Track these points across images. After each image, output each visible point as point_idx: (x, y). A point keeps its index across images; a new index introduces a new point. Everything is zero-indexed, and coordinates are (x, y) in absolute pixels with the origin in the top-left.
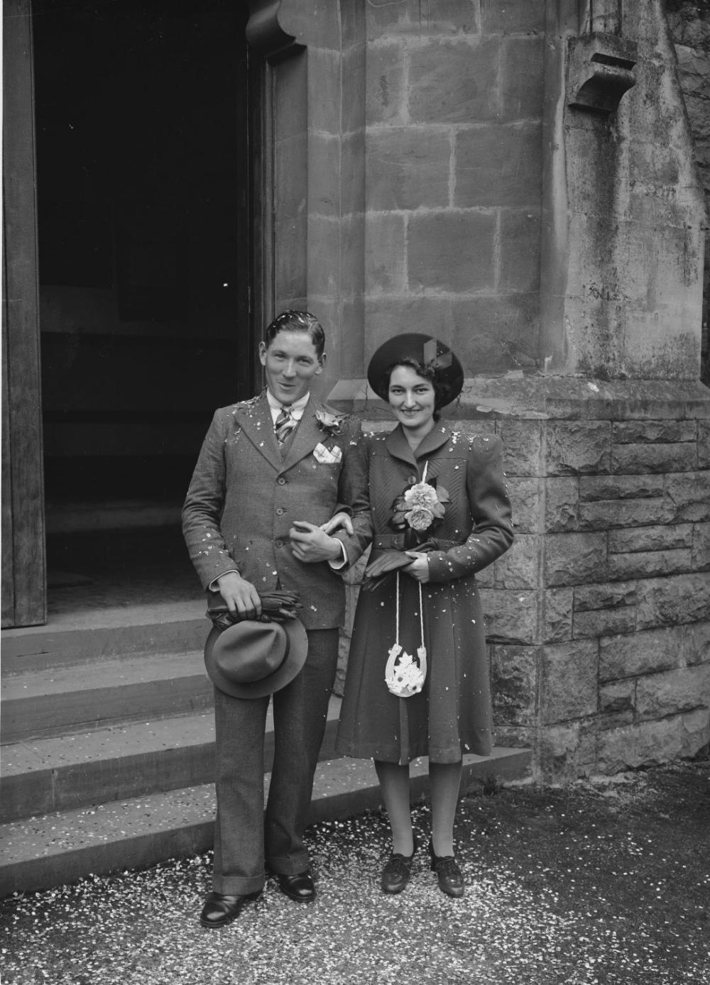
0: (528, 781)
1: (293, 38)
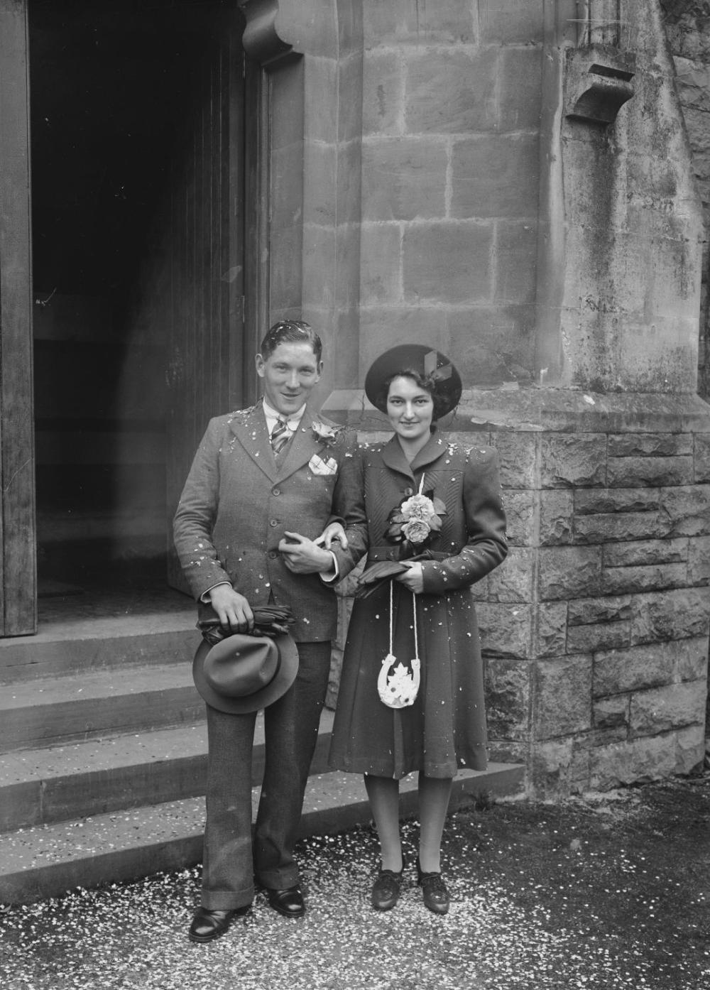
0: (521, 797)
1: (291, 46)
